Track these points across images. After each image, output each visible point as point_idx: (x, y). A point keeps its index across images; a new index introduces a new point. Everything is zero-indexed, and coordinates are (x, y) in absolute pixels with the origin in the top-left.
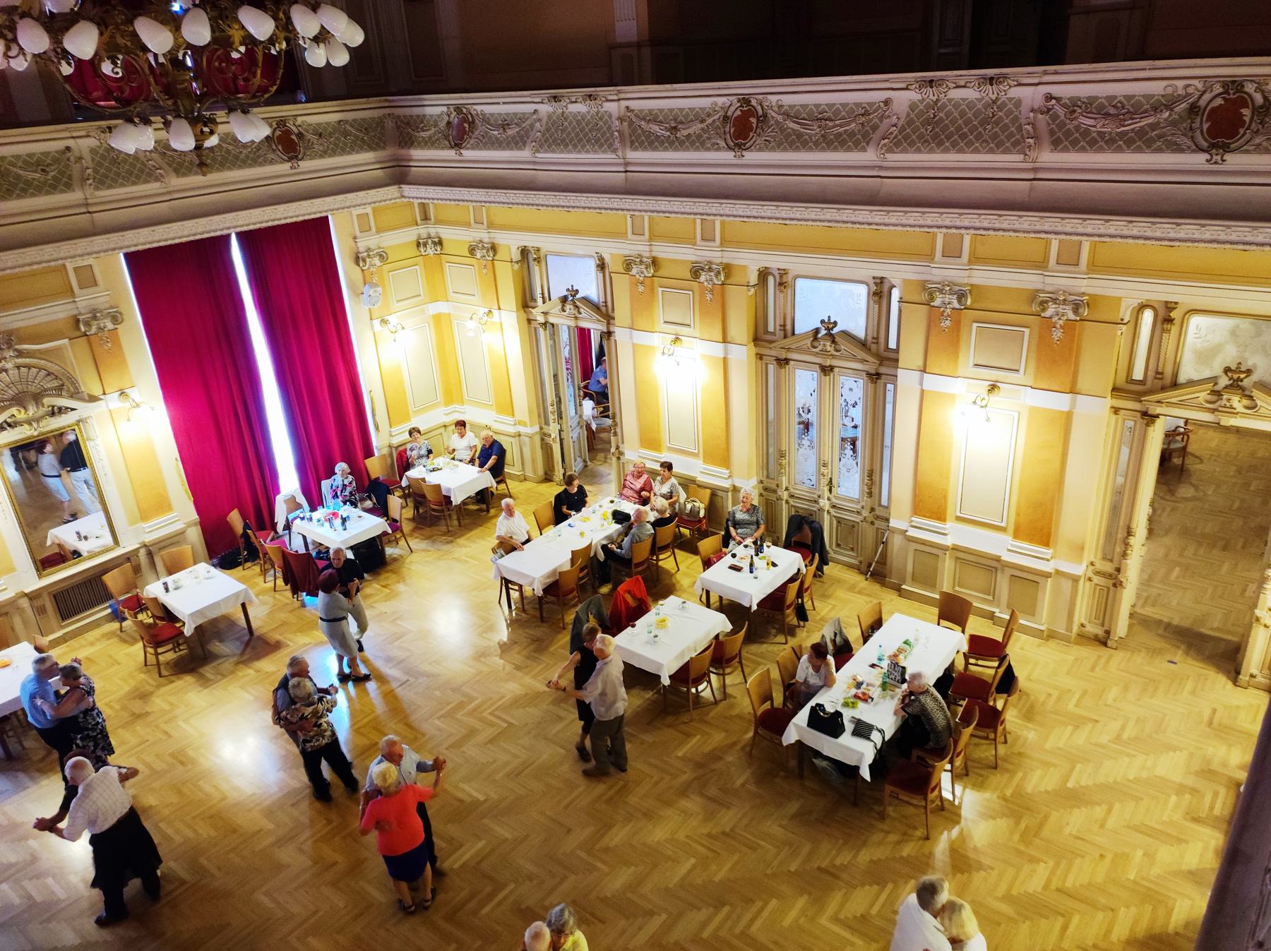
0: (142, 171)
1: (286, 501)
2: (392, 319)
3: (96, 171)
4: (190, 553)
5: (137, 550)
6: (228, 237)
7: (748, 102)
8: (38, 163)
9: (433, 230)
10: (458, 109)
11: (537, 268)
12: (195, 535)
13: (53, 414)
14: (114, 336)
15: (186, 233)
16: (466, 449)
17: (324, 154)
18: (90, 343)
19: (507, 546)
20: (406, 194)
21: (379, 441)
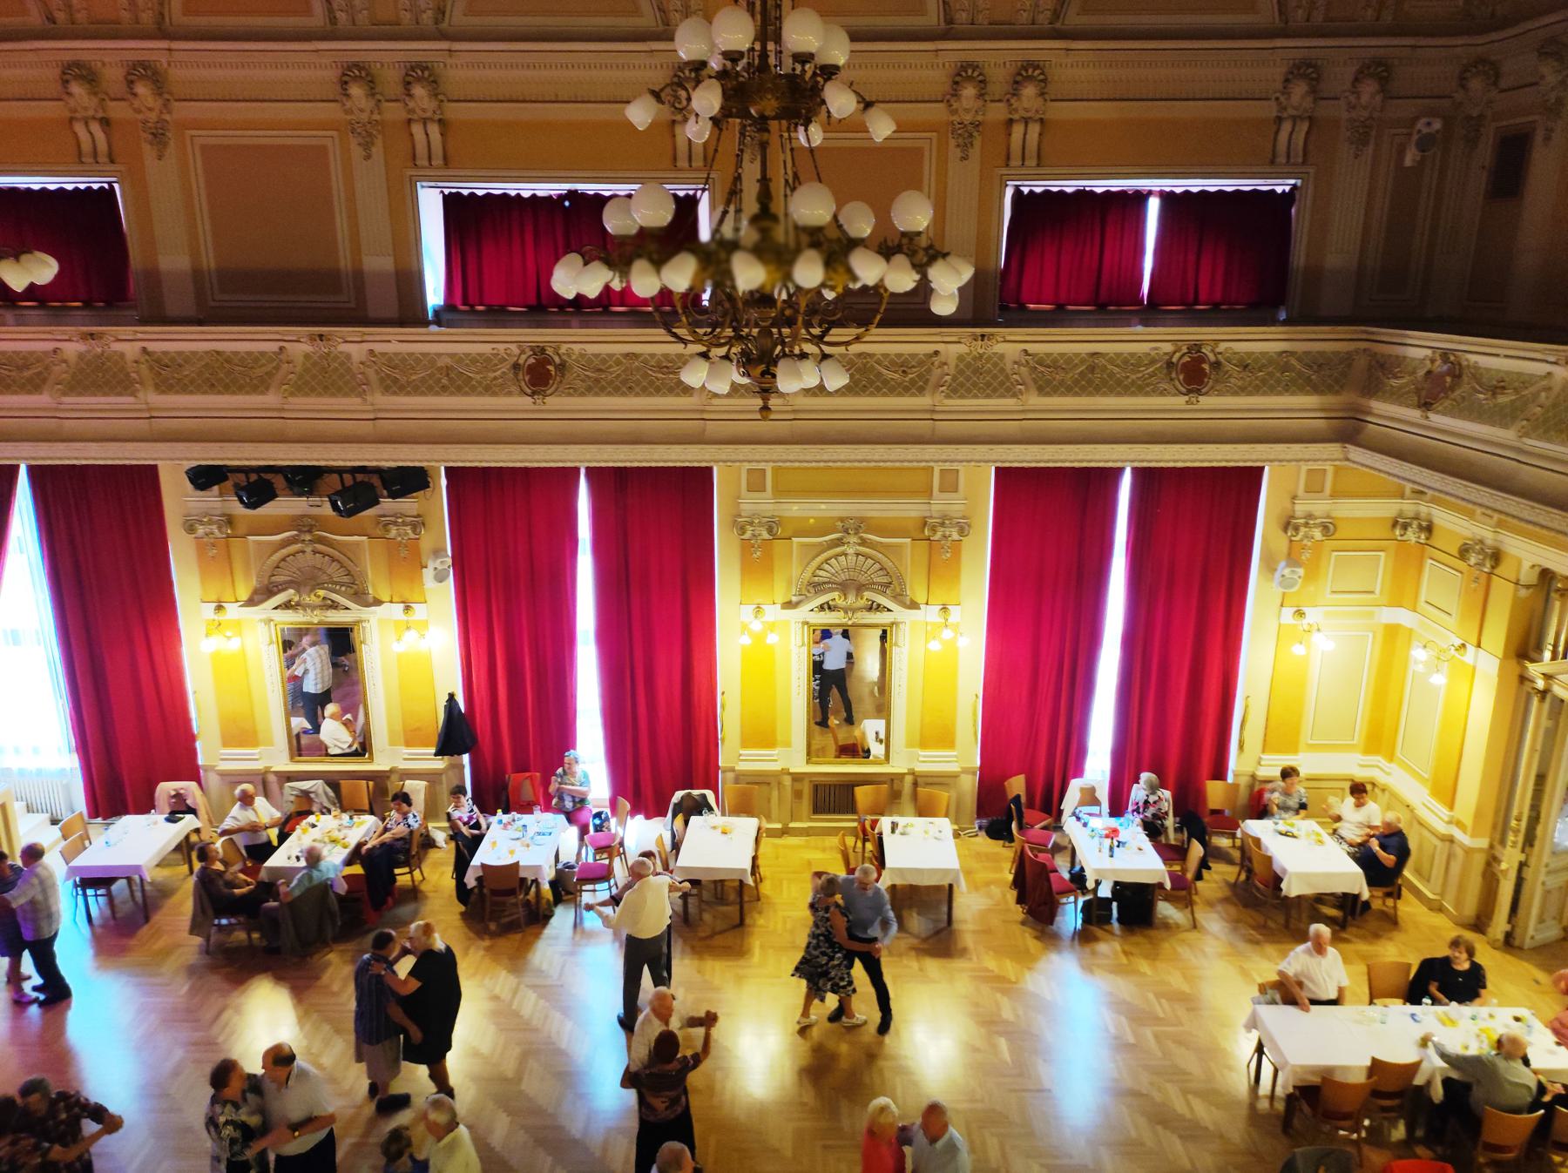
0: (1002, 384)
1: (1082, 790)
2: (1313, 615)
3: (954, 379)
4: (945, 804)
5: (903, 775)
6: (1120, 471)
7: (543, 350)
8: (902, 364)
9: (1424, 509)
10: (1445, 355)
11: (1557, 604)
12: (969, 785)
13: (870, 609)
14: (956, 548)
15: (1028, 458)
16: (1361, 825)
17: (1242, 390)
18: (930, 546)
19: (1287, 993)
20: (1351, 456)
21: (1238, 764)
